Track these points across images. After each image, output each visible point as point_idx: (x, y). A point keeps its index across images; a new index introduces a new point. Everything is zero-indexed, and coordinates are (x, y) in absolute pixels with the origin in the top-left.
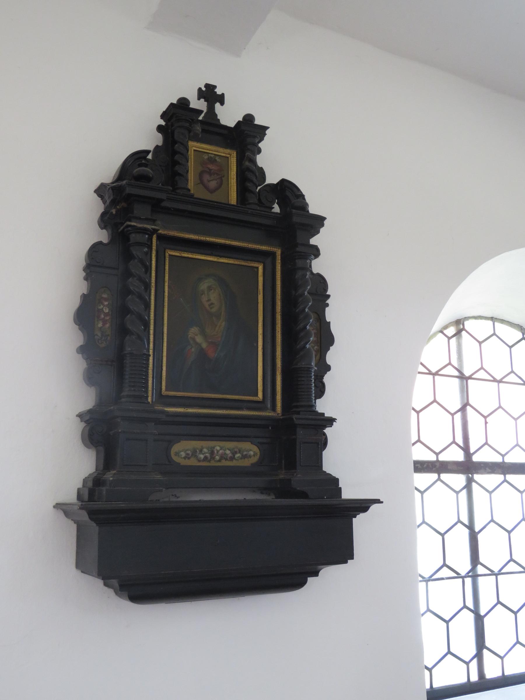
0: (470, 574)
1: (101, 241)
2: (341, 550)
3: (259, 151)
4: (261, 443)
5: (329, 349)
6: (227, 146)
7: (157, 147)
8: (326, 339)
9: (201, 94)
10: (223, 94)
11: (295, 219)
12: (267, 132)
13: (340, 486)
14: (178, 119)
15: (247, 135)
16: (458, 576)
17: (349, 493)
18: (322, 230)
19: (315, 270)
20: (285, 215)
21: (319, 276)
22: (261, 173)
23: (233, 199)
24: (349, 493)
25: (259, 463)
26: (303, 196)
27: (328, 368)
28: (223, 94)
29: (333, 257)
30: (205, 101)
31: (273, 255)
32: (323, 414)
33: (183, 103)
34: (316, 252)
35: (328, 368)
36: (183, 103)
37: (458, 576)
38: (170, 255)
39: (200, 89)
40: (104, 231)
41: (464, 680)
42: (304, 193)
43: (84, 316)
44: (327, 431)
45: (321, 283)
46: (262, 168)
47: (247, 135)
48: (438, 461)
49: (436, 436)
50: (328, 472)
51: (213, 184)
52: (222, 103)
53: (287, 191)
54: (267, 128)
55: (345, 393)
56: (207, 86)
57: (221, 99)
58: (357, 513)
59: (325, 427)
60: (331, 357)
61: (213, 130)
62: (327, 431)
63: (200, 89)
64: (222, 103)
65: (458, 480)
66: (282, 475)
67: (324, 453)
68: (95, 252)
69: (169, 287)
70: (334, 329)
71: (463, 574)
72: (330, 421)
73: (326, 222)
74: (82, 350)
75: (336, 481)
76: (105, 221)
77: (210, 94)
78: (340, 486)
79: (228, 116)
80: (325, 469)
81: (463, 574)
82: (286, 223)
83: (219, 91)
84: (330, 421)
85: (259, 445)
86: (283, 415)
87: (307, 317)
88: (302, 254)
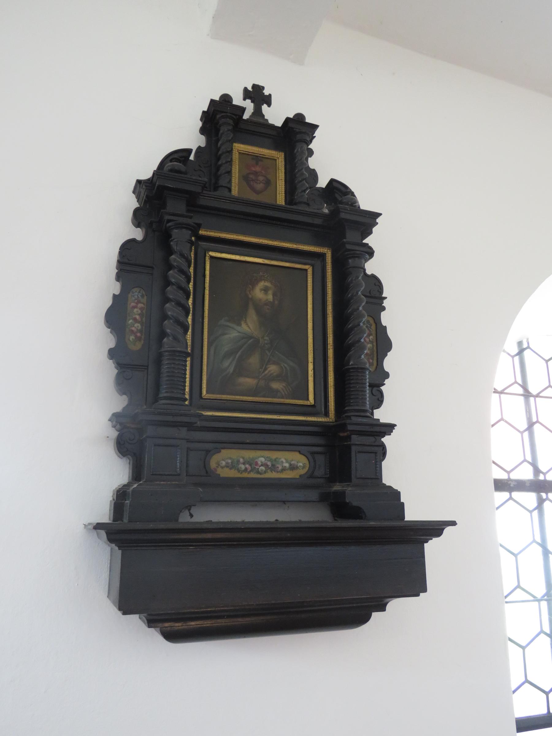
0: (546, 597)
1: (135, 239)
2: (413, 582)
3: (311, 153)
4: (313, 453)
5: (387, 355)
6: (277, 147)
7: (199, 148)
8: (383, 345)
9: (247, 94)
10: (270, 95)
11: (343, 215)
12: (378, 220)
13: (402, 501)
14: (220, 118)
15: (297, 134)
16: (536, 599)
17: (413, 513)
18: (374, 229)
19: (369, 272)
20: (335, 213)
21: (374, 277)
22: (314, 175)
23: (281, 200)
24: (413, 513)
25: (311, 475)
26: (353, 194)
27: (386, 375)
28: (270, 95)
29: (388, 257)
30: (252, 102)
31: (322, 256)
32: (379, 420)
33: (226, 99)
34: (370, 253)
35: (386, 375)
36: (226, 99)
37: (536, 599)
38: (212, 258)
39: (246, 89)
40: (139, 229)
41: (545, 711)
42: (353, 190)
43: (115, 317)
44: (386, 440)
45: (375, 283)
46: (314, 170)
47: (297, 134)
48: (509, 479)
49: (507, 454)
50: (388, 484)
51: (259, 186)
52: (269, 105)
53: (338, 191)
54: (379, 215)
55: (404, 400)
56: (254, 86)
57: (268, 100)
58: (428, 538)
59: (384, 434)
60: (388, 364)
61: (258, 130)
62: (386, 440)
63: (246, 89)
64: (269, 105)
65: (529, 499)
66: (337, 487)
67: (384, 463)
68: (128, 249)
69: (275, 398)
70: (390, 333)
71: (539, 596)
72: (389, 428)
73: (317, 133)
74: (112, 354)
75: (396, 494)
76: (138, 218)
77: (257, 95)
78: (402, 501)
79: (275, 115)
80: (384, 481)
81: (539, 596)
82: (339, 225)
83: (266, 92)
84: (389, 428)
85: (312, 456)
86: (336, 421)
87: (361, 316)
88: (352, 252)
